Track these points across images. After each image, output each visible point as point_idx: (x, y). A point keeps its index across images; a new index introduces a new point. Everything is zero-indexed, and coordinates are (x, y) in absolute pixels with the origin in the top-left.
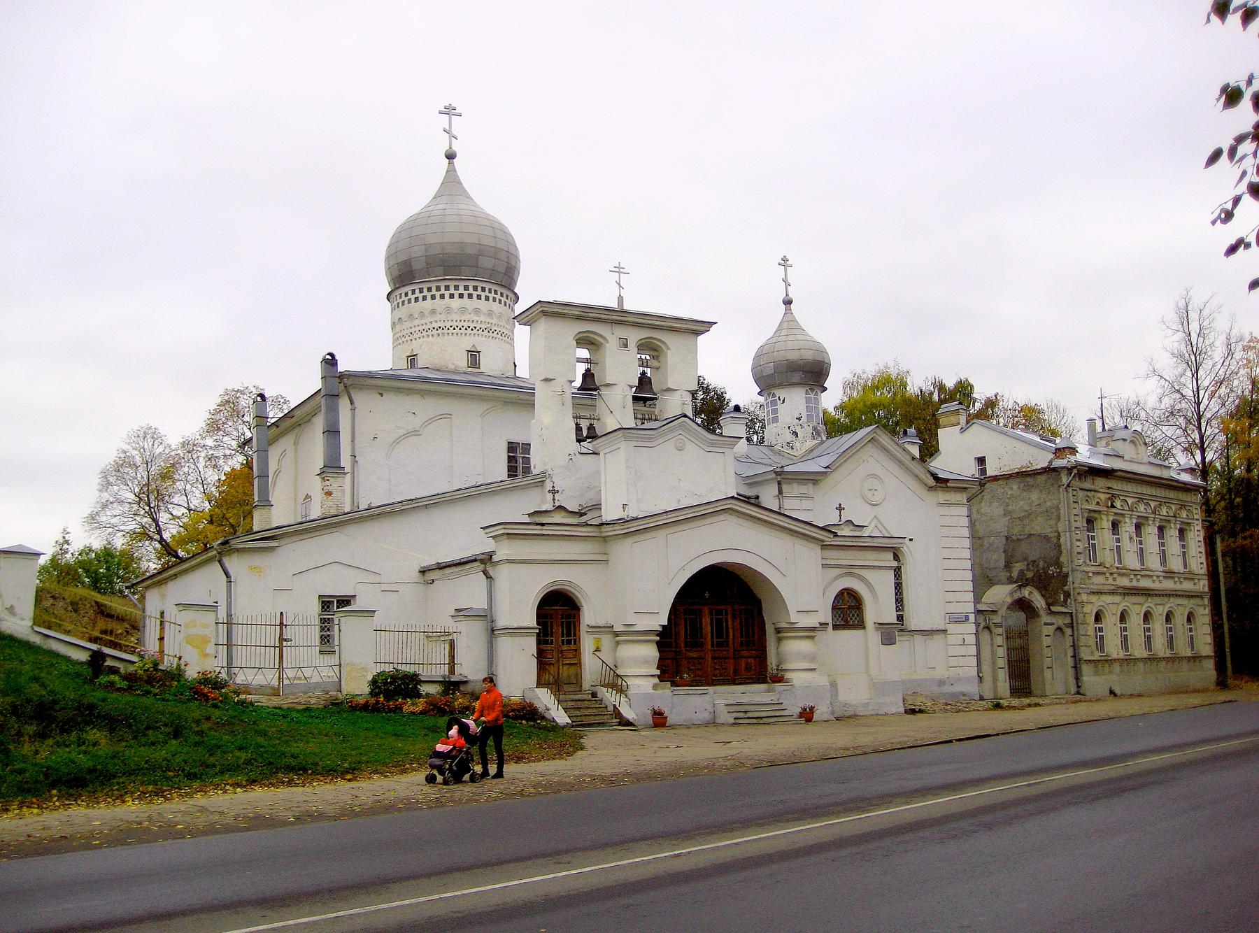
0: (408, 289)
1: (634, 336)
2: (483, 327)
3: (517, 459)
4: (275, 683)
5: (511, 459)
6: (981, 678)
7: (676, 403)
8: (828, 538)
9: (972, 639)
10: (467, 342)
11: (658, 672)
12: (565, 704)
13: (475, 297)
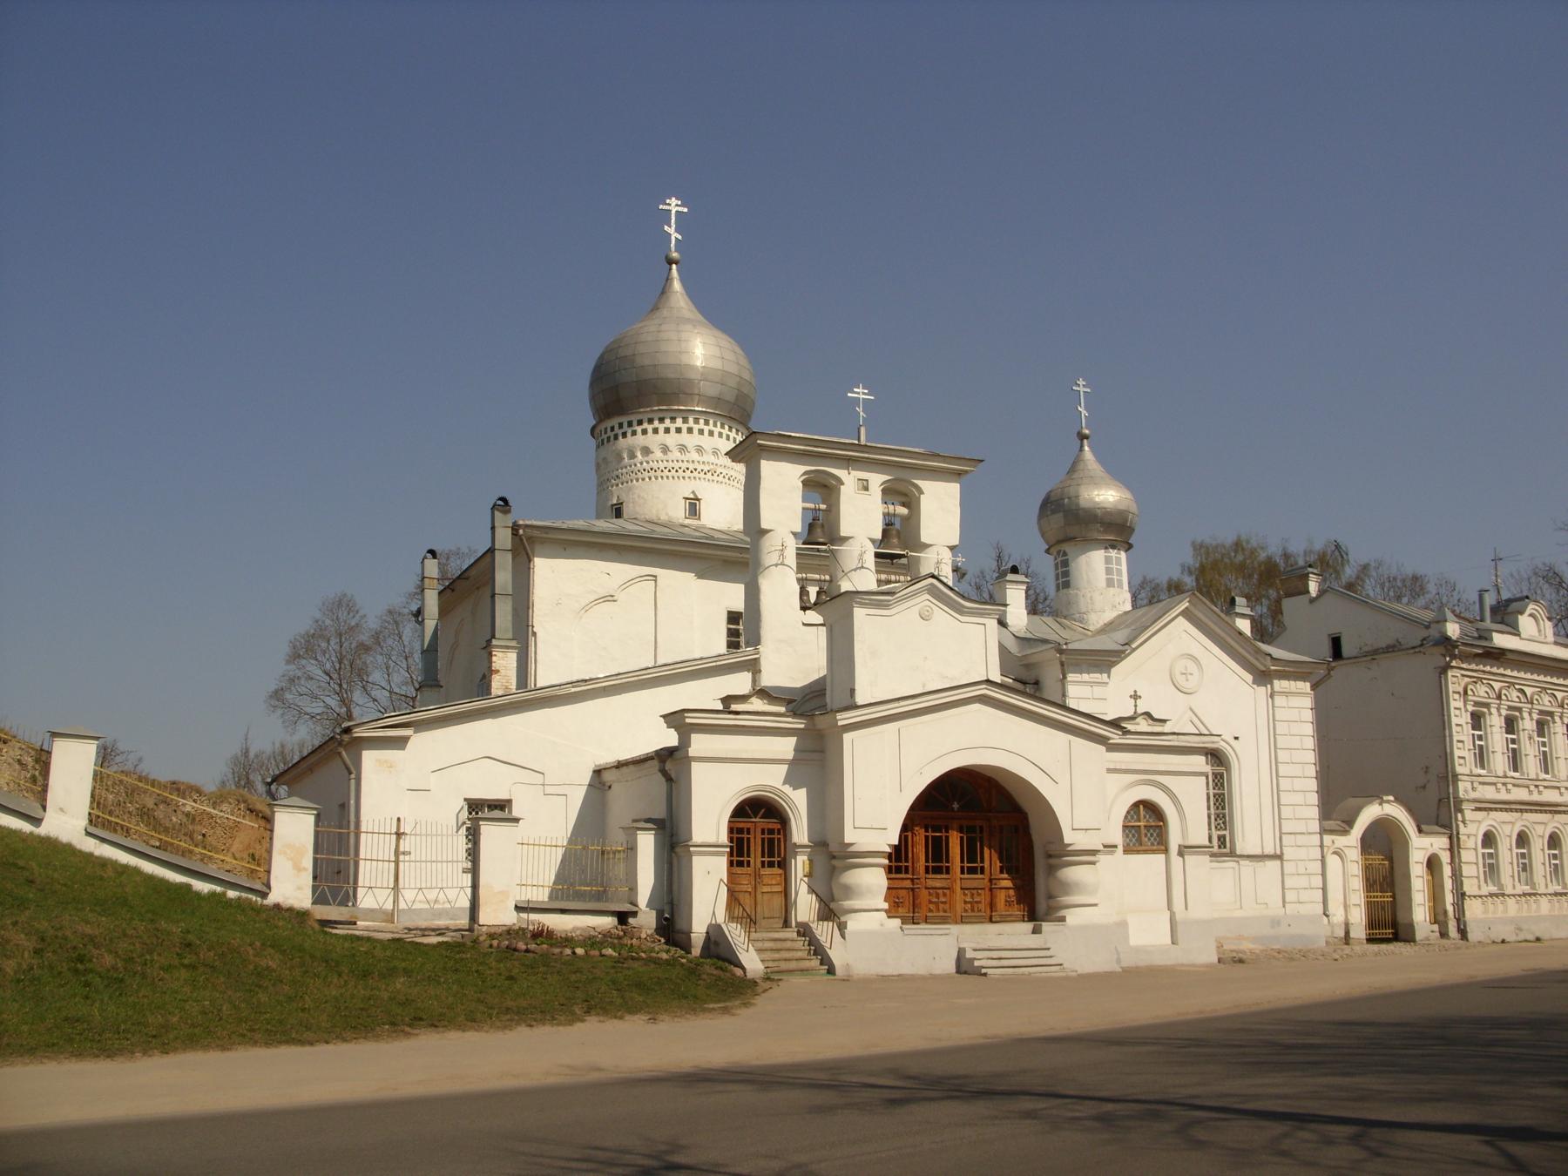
0: (615, 422)
1: (877, 480)
2: (706, 468)
3: (742, 629)
4: (389, 906)
5: (733, 634)
8: (1111, 733)
10: (686, 488)
11: (886, 906)
12: (760, 945)
13: (696, 431)
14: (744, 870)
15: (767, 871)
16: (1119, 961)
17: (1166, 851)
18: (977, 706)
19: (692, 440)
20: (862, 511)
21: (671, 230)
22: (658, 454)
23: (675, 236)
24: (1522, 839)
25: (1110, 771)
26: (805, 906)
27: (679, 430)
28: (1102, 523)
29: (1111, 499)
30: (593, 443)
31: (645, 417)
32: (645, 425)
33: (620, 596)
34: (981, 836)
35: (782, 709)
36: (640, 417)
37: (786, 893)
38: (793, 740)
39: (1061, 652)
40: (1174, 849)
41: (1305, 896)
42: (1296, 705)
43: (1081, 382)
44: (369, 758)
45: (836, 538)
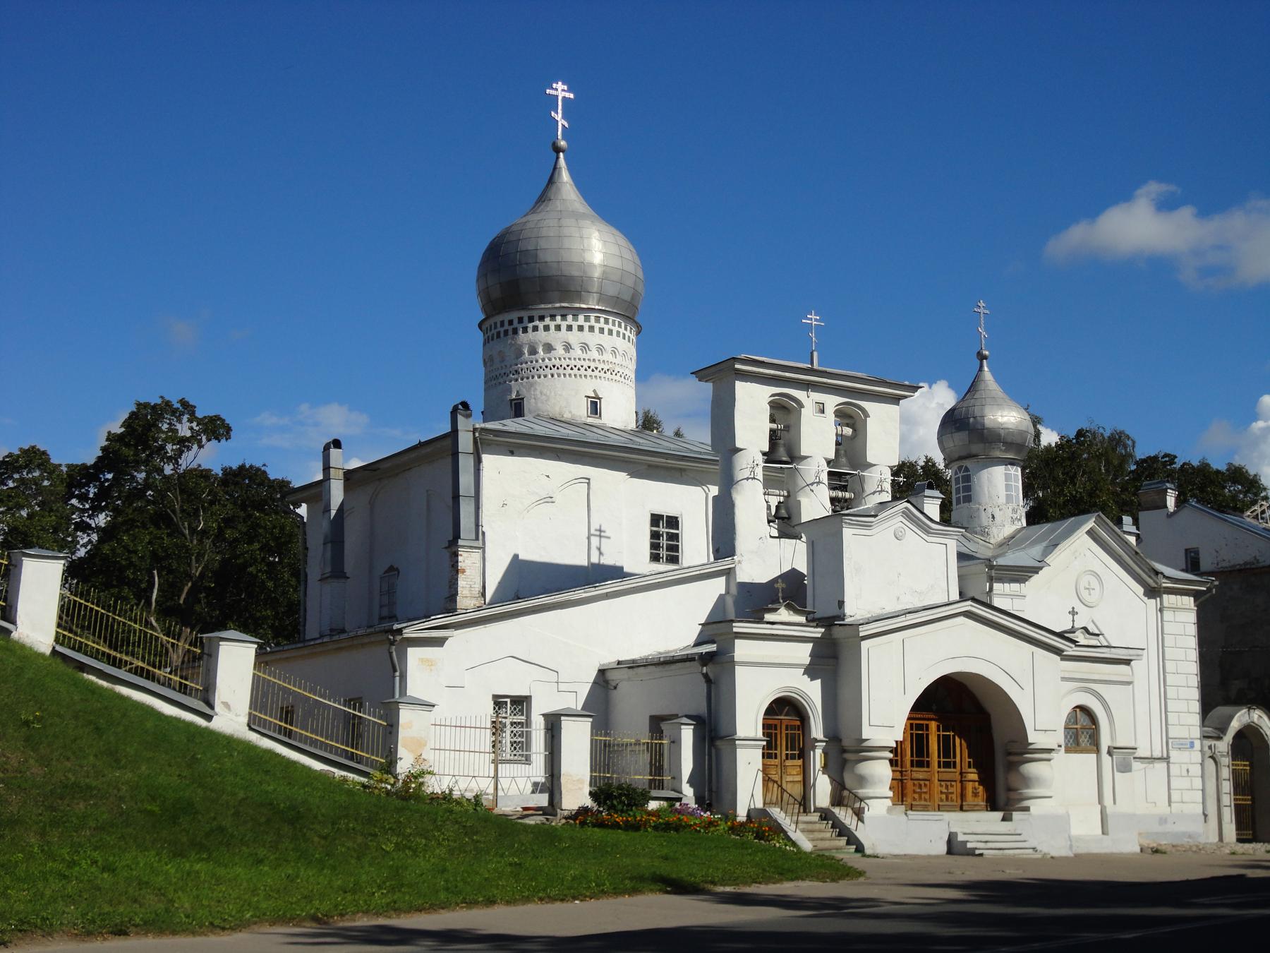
1: (832, 402)
6: (1205, 816)
7: (878, 480)
8: (1056, 642)
9: (1196, 770)
10: (588, 387)
11: (891, 794)
14: (773, 761)
15: (789, 763)
16: (1071, 847)
17: (1098, 751)
18: (962, 619)
19: (593, 339)
20: (818, 435)
21: (559, 117)
22: (560, 351)
25: (1064, 679)
27: (581, 328)
28: (1005, 443)
29: (1012, 420)
30: (480, 336)
31: (536, 314)
32: (537, 323)
33: (558, 498)
34: (967, 733)
35: (802, 619)
36: (541, 313)
38: (809, 647)
39: (991, 567)
40: (1104, 749)
41: (1187, 796)
42: (1182, 618)
43: (982, 304)
44: (413, 654)
45: (795, 457)
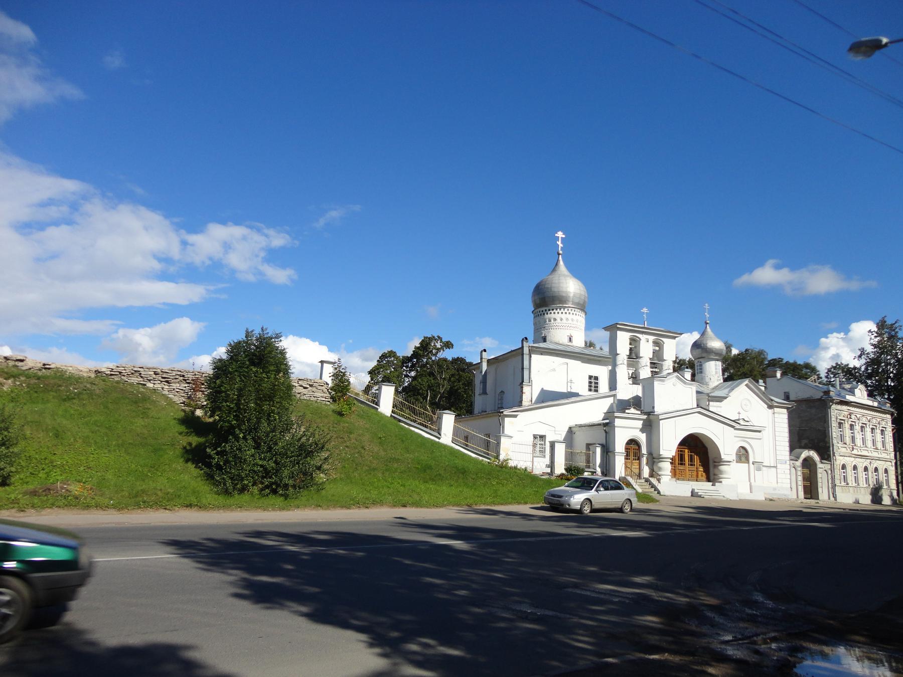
1: (652, 338)
8: (733, 424)
10: (568, 333)
17: (748, 463)
19: (570, 317)
20: (646, 349)
23: (561, 245)
24: (855, 468)
26: (646, 472)
30: (532, 316)
34: (698, 454)
37: (640, 468)
40: (751, 462)
42: (782, 416)
45: (638, 357)
